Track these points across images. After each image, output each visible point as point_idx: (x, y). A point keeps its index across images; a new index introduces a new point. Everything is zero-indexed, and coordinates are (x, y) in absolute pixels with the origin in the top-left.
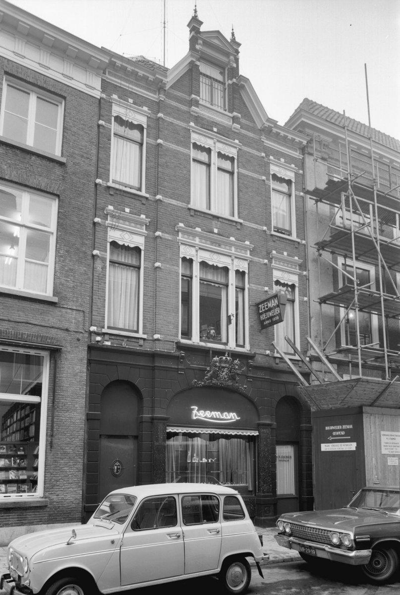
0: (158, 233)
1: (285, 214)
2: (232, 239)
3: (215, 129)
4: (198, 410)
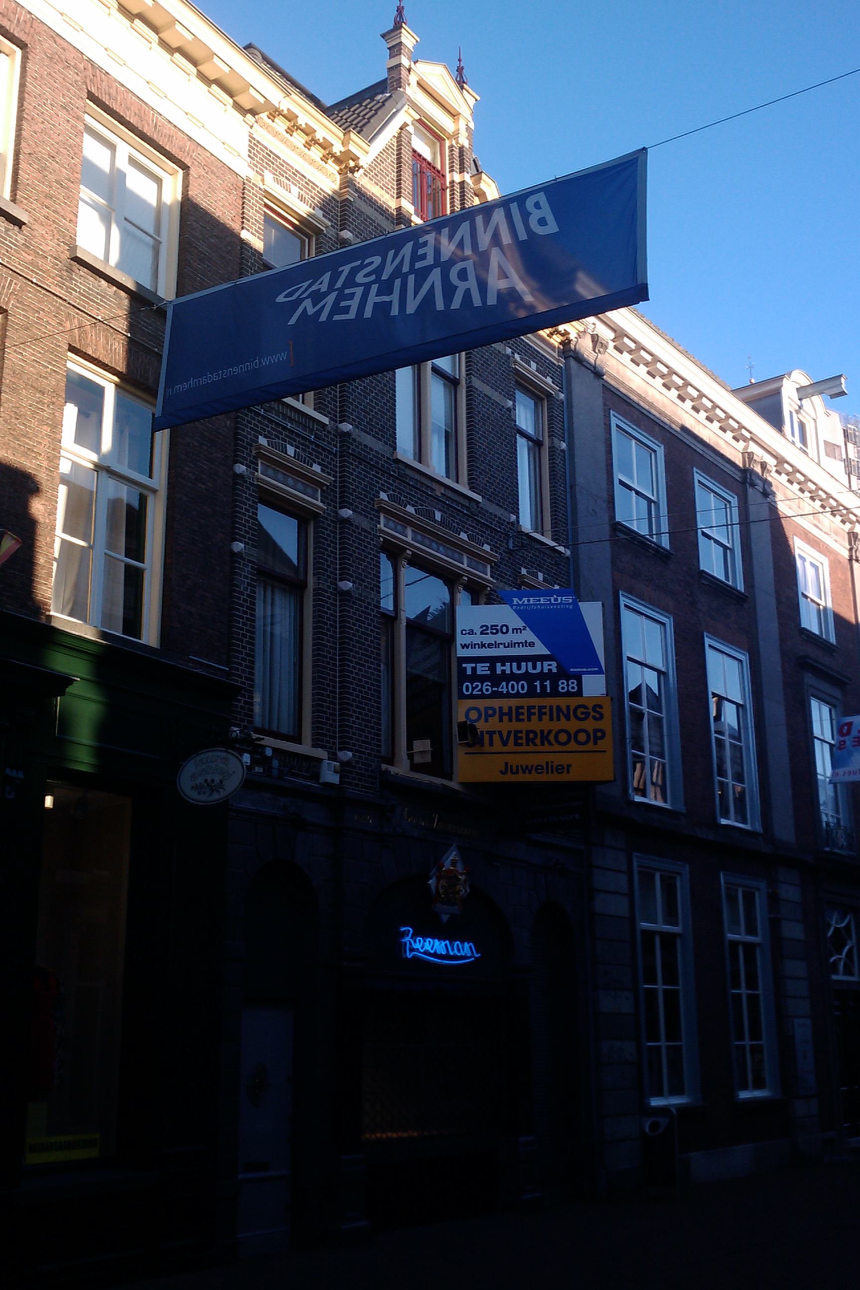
0: (347, 513)
2: (410, 509)
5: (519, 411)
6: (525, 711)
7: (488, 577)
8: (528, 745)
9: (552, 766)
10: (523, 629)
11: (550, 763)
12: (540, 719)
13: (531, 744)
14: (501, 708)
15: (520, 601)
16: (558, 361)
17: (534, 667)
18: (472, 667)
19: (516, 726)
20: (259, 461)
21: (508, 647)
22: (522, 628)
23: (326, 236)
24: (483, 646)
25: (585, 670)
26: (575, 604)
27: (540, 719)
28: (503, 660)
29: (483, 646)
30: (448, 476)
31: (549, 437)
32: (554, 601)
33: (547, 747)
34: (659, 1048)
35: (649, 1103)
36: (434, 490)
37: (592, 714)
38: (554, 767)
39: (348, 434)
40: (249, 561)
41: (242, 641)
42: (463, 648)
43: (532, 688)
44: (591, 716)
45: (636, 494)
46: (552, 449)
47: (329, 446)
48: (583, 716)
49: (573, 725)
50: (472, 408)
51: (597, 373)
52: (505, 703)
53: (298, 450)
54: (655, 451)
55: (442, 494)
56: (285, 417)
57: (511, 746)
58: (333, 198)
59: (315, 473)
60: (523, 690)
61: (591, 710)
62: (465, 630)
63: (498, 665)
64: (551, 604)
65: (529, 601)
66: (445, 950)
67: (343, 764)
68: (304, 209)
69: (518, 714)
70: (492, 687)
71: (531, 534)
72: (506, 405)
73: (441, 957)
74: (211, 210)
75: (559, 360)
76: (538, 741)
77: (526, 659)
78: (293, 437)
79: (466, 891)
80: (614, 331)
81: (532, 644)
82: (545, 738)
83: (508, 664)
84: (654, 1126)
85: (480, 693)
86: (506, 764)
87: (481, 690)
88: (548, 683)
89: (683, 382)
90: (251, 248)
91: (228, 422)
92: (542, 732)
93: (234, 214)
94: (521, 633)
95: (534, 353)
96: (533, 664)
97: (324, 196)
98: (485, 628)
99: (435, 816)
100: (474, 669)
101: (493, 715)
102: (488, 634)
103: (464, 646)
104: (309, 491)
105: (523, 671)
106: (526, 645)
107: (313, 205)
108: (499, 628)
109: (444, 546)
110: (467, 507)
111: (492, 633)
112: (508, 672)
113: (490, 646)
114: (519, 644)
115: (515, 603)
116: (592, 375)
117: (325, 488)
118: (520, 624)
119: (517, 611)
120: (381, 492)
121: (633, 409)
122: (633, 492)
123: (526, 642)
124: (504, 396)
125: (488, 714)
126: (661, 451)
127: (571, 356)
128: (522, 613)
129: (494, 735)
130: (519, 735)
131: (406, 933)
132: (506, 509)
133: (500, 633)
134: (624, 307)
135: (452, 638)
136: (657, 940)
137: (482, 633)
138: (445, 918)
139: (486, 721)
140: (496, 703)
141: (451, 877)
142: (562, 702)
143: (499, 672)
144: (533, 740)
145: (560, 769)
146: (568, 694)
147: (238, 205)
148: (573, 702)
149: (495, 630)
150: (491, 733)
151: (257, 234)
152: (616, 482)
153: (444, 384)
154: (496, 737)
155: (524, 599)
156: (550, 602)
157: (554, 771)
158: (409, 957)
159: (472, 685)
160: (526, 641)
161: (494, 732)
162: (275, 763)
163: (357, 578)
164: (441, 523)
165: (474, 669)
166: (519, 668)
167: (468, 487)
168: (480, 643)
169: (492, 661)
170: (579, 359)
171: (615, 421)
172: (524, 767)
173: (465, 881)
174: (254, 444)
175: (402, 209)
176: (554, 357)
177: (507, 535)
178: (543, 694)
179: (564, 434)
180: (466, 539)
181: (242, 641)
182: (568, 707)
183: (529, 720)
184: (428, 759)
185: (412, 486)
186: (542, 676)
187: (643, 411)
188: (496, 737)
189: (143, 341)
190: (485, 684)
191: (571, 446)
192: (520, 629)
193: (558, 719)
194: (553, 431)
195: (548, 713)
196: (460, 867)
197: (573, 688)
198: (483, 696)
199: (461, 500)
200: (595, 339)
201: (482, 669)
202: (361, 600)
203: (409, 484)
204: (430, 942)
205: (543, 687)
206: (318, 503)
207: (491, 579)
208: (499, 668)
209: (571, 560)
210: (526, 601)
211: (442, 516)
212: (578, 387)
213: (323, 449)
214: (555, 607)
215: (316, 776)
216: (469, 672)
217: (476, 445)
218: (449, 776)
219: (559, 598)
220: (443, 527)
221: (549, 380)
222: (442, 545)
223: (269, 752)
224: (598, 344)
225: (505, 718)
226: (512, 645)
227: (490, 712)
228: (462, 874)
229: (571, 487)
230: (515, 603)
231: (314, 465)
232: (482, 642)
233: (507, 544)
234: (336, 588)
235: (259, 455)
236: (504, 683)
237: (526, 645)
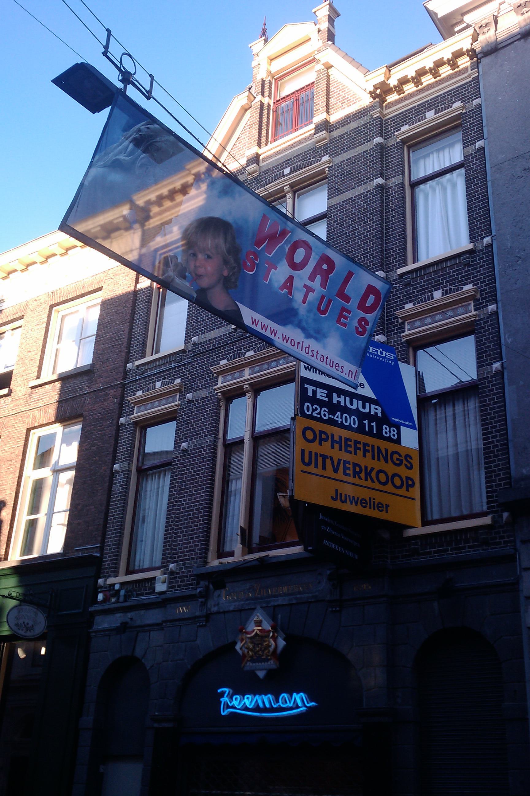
9: (374, 502)
12: (364, 456)
18: (313, 390)
25: (403, 422)
26: (396, 361)
27: (364, 456)
28: (340, 392)
33: (369, 483)
37: (405, 462)
42: (306, 369)
44: (403, 464)
48: (398, 462)
49: (391, 469)
57: (340, 475)
61: (403, 458)
63: (335, 395)
64: (377, 355)
76: (363, 475)
83: (342, 397)
85: (319, 416)
87: (320, 413)
88: (374, 424)
101: (326, 440)
105: (354, 407)
134: (77, 461)
142: (383, 445)
143: (335, 402)
145: (380, 507)
146: (389, 439)
148: (392, 447)
156: (377, 353)
157: (376, 508)
165: (314, 392)
169: (331, 390)
172: (351, 497)
178: (370, 433)
182: (386, 450)
193: (379, 460)
197: (386, 428)
198: (320, 420)
201: (321, 394)
205: (371, 427)
214: (381, 359)
216: (310, 394)
219: (384, 352)
236: (339, 414)
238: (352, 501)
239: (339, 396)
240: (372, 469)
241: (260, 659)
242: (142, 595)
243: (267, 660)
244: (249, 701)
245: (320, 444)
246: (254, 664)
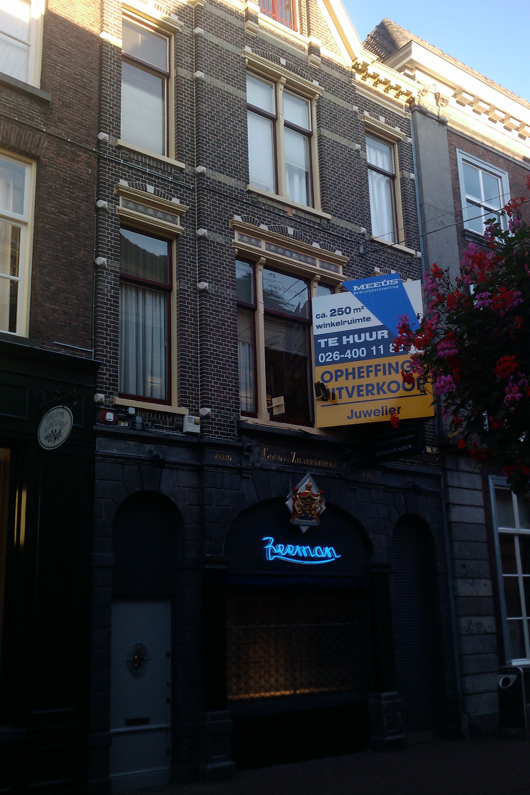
0: (202, 232)
1: (479, 247)
2: (316, 245)
3: (283, 61)
4: (274, 544)
5: (370, 154)
6: (365, 370)
7: (179, 226)
8: (367, 395)
9: (386, 409)
10: (362, 309)
11: (384, 407)
12: (376, 375)
13: (369, 394)
14: (347, 370)
15: (359, 287)
16: (405, 114)
17: (371, 336)
19: (358, 382)
20: (121, 198)
21: (351, 323)
22: (361, 308)
23: (181, 33)
24: (333, 324)
26: (400, 284)
27: (376, 375)
28: (347, 333)
29: (333, 324)
30: (308, 205)
31: (400, 170)
32: (385, 284)
33: (382, 396)
34: (521, 622)
35: (511, 663)
36: (287, 212)
38: (388, 410)
39: (202, 174)
40: (111, 271)
41: (106, 330)
43: (370, 353)
45: (484, 209)
46: (403, 179)
47: (188, 184)
50: (322, 151)
51: (442, 122)
52: (350, 366)
53: (157, 188)
54: (500, 177)
55: (293, 214)
56: (145, 164)
57: (355, 398)
58: (187, 6)
59: (338, 256)
60: (363, 354)
62: (319, 315)
65: (365, 287)
66: (306, 554)
67: (203, 418)
68: (160, 16)
69: (360, 372)
70: (340, 354)
71: (394, 246)
72: (355, 148)
73: (303, 558)
74: (70, 18)
75: (406, 114)
76: (375, 391)
77: (364, 330)
78: (152, 179)
79: (321, 509)
80: (454, 89)
81: (368, 319)
82: (380, 388)
83: (351, 336)
84: (505, 682)
85: (331, 360)
86: (352, 411)
87: (332, 358)
88: (381, 347)
89: (520, 123)
90: (111, 45)
91: (90, 170)
92: (378, 384)
93: (93, 20)
94: (360, 311)
95: (398, 118)
96: (370, 334)
97: (179, 5)
98: (333, 311)
99: (293, 454)
100: (326, 343)
102: (336, 315)
103: (319, 327)
104: (169, 217)
105: (363, 340)
106: (364, 320)
107: (169, 12)
108: (343, 310)
109: (297, 253)
110: (317, 223)
111: (339, 314)
112: (351, 342)
113: (338, 324)
114: (359, 320)
115: (355, 290)
116: (437, 123)
117: (345, 265)
118: (359, 304)
119: (356, 295)
120: (235, 215)
121: (477, 147)
122: (482, 209)
123: (364, 318)
124: (352, 141)
125: (338, 375)
126: (505, 177)
127: (416, 110)
128: (360, 297)
129: (342, 390)
130: (361, 388)
131: (267, 542)
132: (356, 224)
133: (344, 313)
135: (309, 323)
136: (517, 541)
137: (331, 315)
138: (304, 529)
139: (336, 380)
140: (342, 366)
141: (308, 499)
143: (345, 343)
144: (371, 391)
147: (97, 14)
149: (341, 311)
150: (340, 389)
151: (116, 35)
152: (464, 204)
153: (304, 138)
154: (344, 392)
155: (361, 286)
156: (381, 285)
158: (271, 560)
159: (325, 355)
160: (364, 317)
161: (343, 388)
162: (139, 419)
163: (212, 279)
164: (295, 236)
165: (326, 343)
166: (360, 338)
167: (321, 210)
168: (330, 323)
169: (339, 335)
170: (424, 112)
171: (460, 156)
172: (365, 413)
173: (320, 501)
174: (115, 185)
175: (249, 9)
176: (402, 113)
177: (358, 243)
178: (379, 355)
179: (413, 168)
180: (319, 247)
181: (106, 330)
183: (368, 376)
184: (283, 411)
185: (265, 210)
186: (377, 342)
187: (488, 148)
188: (344, 392)
189: (5, 113)
190: (335, 353)
191: (419, 176)
192: (359, 308)
193: (390, 373)
194: (403, 166)
195: (382, 370)
196: (314, 491)
198: (334, 362)
199: (313, 219)
200: (437, 97)
201: (332, 342)
202: (218, 296)
203: (262, 209)
204: (291, 548)
205: (378, 350)
206: (177, 226)
207: (344, 276)
208: (345, 340)
209: (423, 261)
210: (363, 287)
211: (294, 231)
212: (422, 133)
213: (181, 186)
214: (385, 289)
215: (180, 428)
216: (323, 346)
217: (326, 178)
218: (312, 425)
219: (388, 282)
220: (296, 239)
221: (397, 129)
222: (295, 253)
223: (132, 411)
224: (440, 99)
225: (350, 377)
226: (354, 321)
227: (339, 373)
228: (317, 496)
229: (421, 206)
230: (355, 290)
231: (173, 199)
232: (331, 322)
233: (358, 249)
234: (196, 289)
235: (120, 193)
236: (349, 351)
237: (364, 320)
238: (366, 414)
239: (348, 337)
240: (384, 383)
241: (306, 517)
242: (162, 428)
243: (312, 519)
244: (290, 550)
245: (336, 380)
246: (301, 520)
